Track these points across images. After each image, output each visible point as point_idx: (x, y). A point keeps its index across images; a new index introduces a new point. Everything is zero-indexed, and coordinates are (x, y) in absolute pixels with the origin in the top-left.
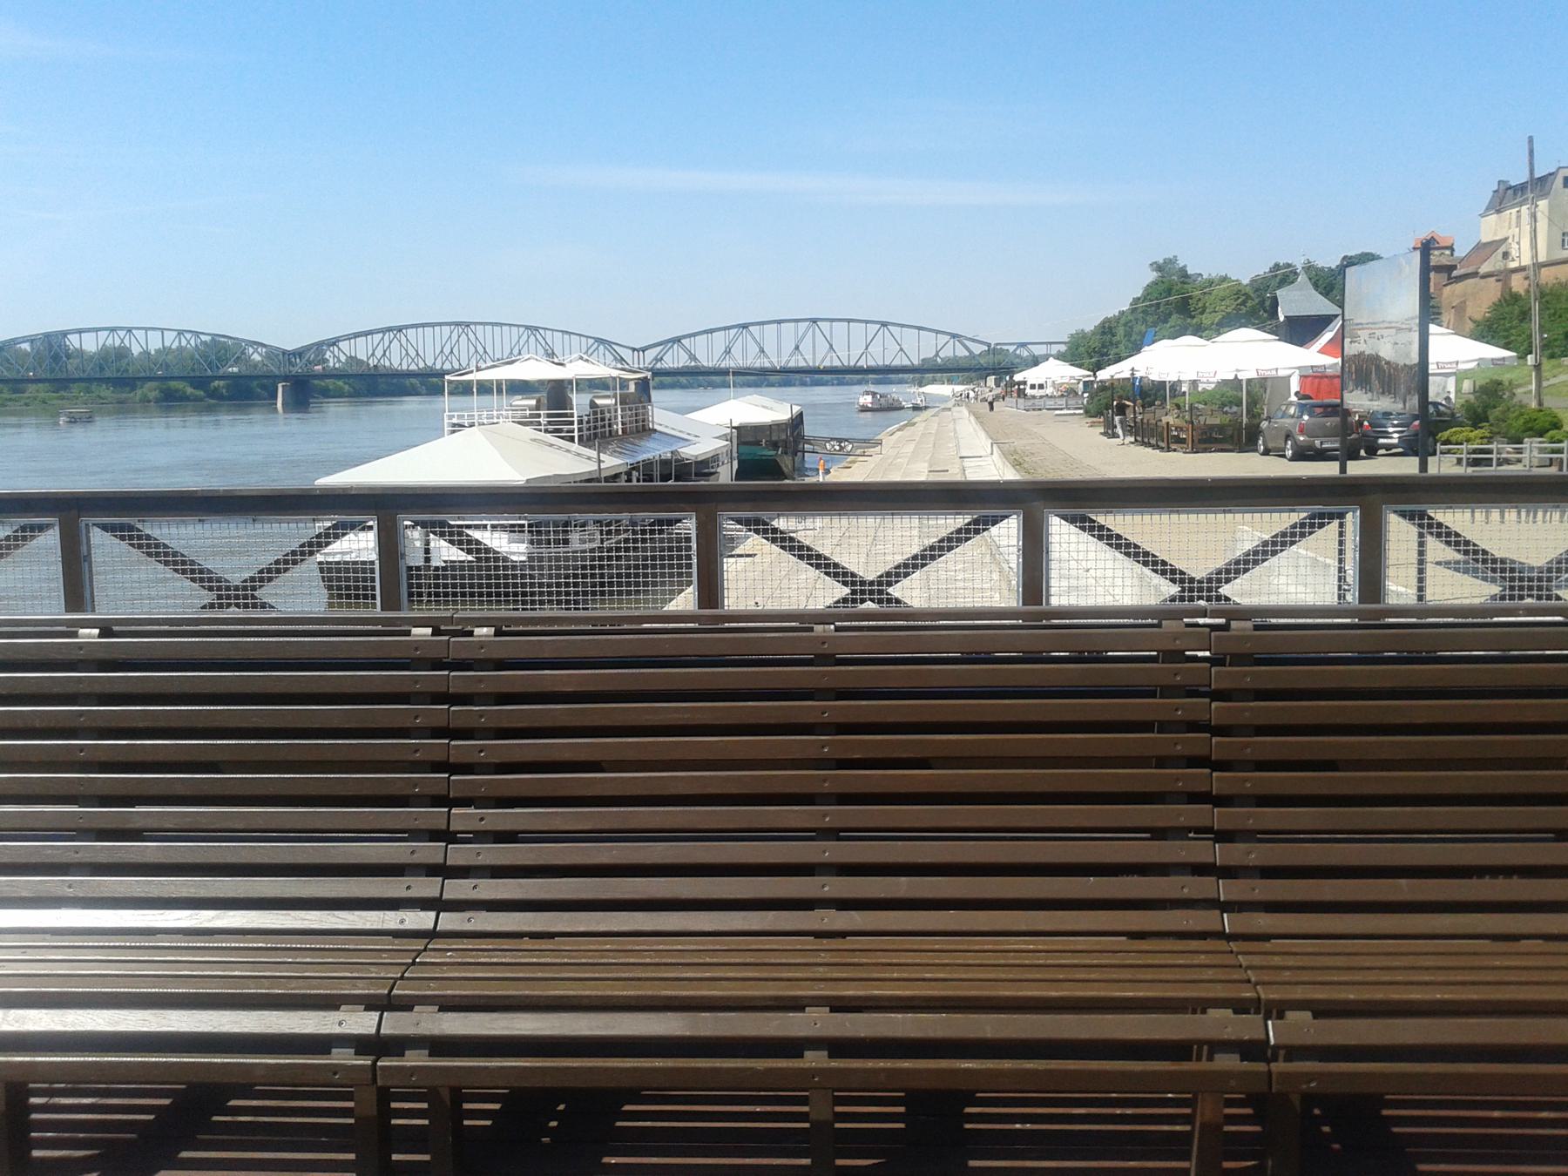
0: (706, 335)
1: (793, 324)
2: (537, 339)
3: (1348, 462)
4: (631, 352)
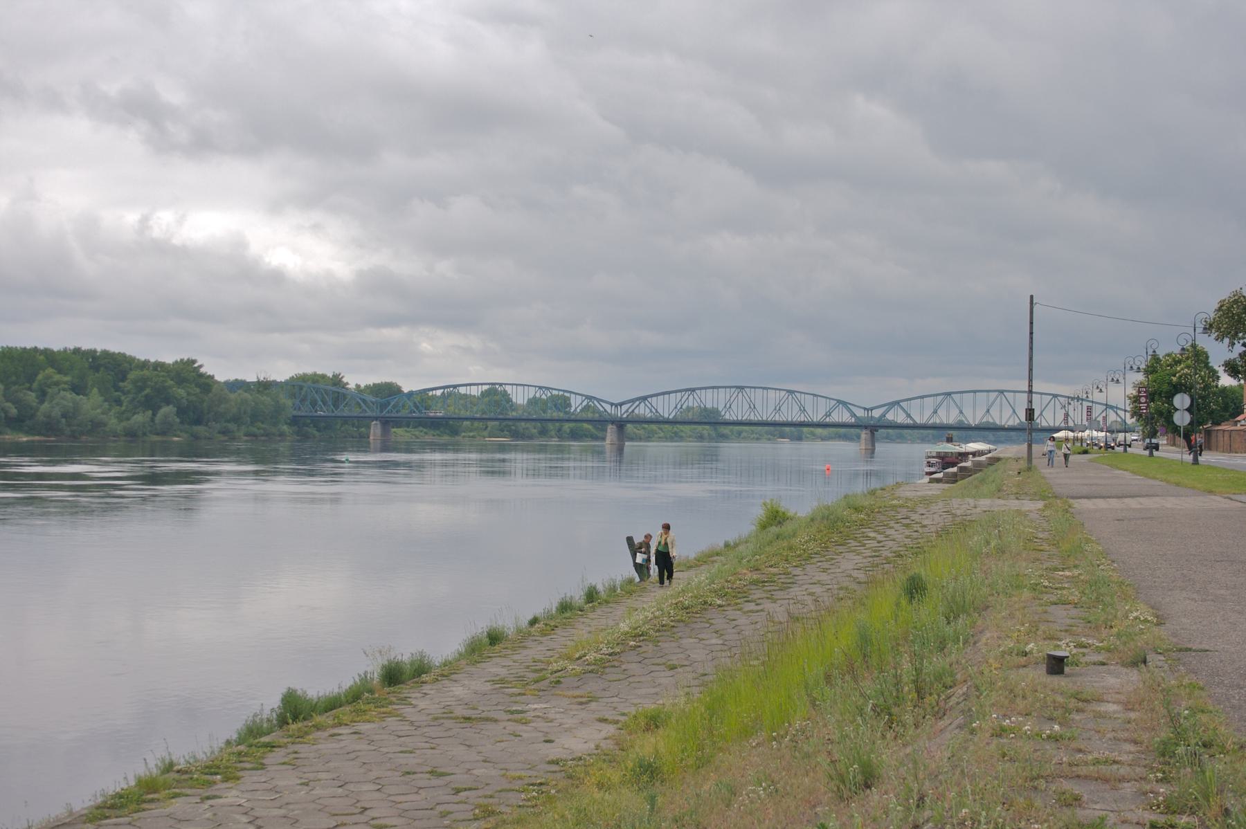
0: (919, 400)
1: (986, 393)
2: (743, 395)
4: (863, 410)
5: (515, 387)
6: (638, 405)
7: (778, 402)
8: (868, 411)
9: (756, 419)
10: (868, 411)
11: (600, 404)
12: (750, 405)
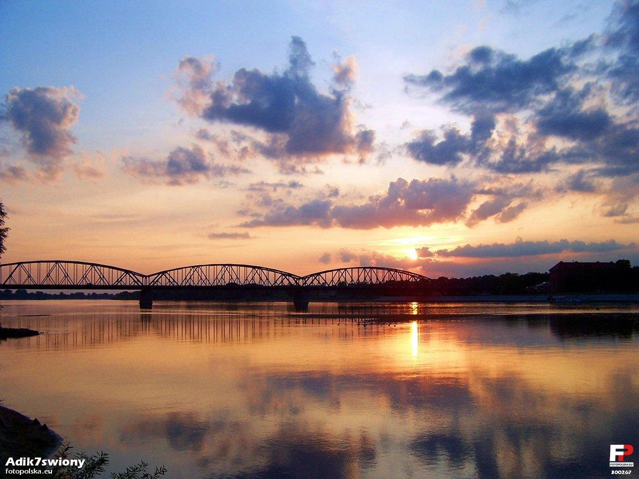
3: (611, 445)
5: (208, 267)
6: (161, 277)
7: (84, 273)
8: (146, 278)
9: (69, 284)
10: (146, 278)
11: (136, 277)
12: (100, 276)
